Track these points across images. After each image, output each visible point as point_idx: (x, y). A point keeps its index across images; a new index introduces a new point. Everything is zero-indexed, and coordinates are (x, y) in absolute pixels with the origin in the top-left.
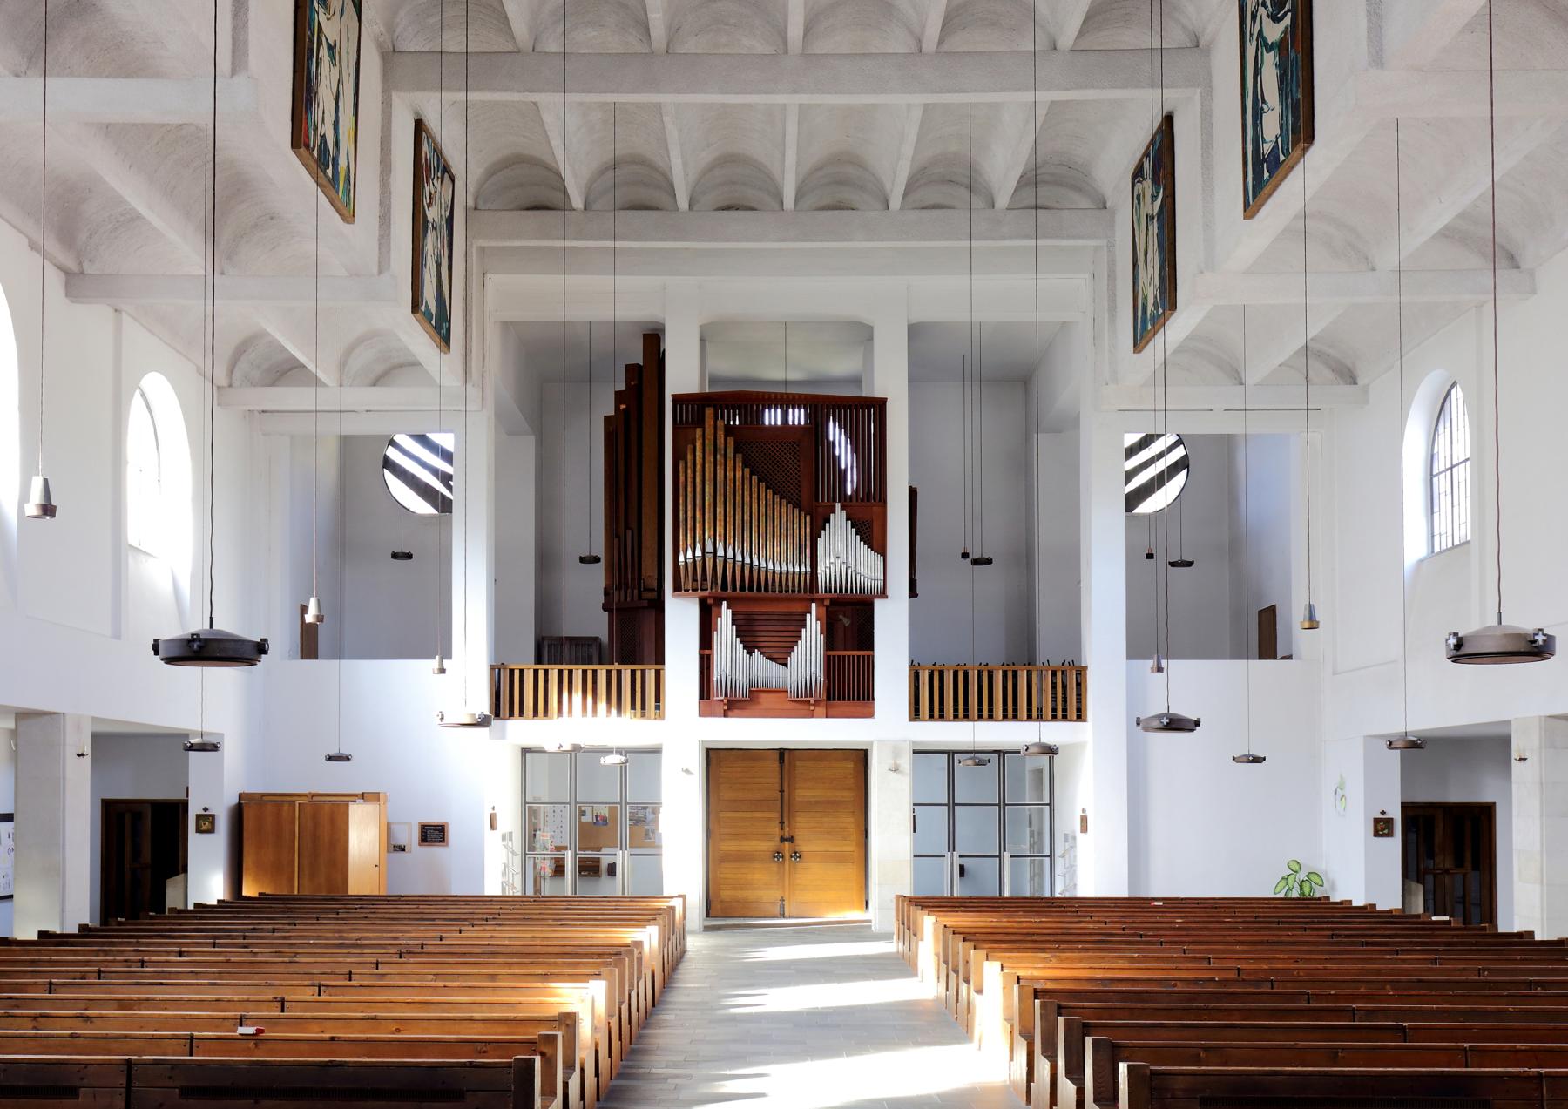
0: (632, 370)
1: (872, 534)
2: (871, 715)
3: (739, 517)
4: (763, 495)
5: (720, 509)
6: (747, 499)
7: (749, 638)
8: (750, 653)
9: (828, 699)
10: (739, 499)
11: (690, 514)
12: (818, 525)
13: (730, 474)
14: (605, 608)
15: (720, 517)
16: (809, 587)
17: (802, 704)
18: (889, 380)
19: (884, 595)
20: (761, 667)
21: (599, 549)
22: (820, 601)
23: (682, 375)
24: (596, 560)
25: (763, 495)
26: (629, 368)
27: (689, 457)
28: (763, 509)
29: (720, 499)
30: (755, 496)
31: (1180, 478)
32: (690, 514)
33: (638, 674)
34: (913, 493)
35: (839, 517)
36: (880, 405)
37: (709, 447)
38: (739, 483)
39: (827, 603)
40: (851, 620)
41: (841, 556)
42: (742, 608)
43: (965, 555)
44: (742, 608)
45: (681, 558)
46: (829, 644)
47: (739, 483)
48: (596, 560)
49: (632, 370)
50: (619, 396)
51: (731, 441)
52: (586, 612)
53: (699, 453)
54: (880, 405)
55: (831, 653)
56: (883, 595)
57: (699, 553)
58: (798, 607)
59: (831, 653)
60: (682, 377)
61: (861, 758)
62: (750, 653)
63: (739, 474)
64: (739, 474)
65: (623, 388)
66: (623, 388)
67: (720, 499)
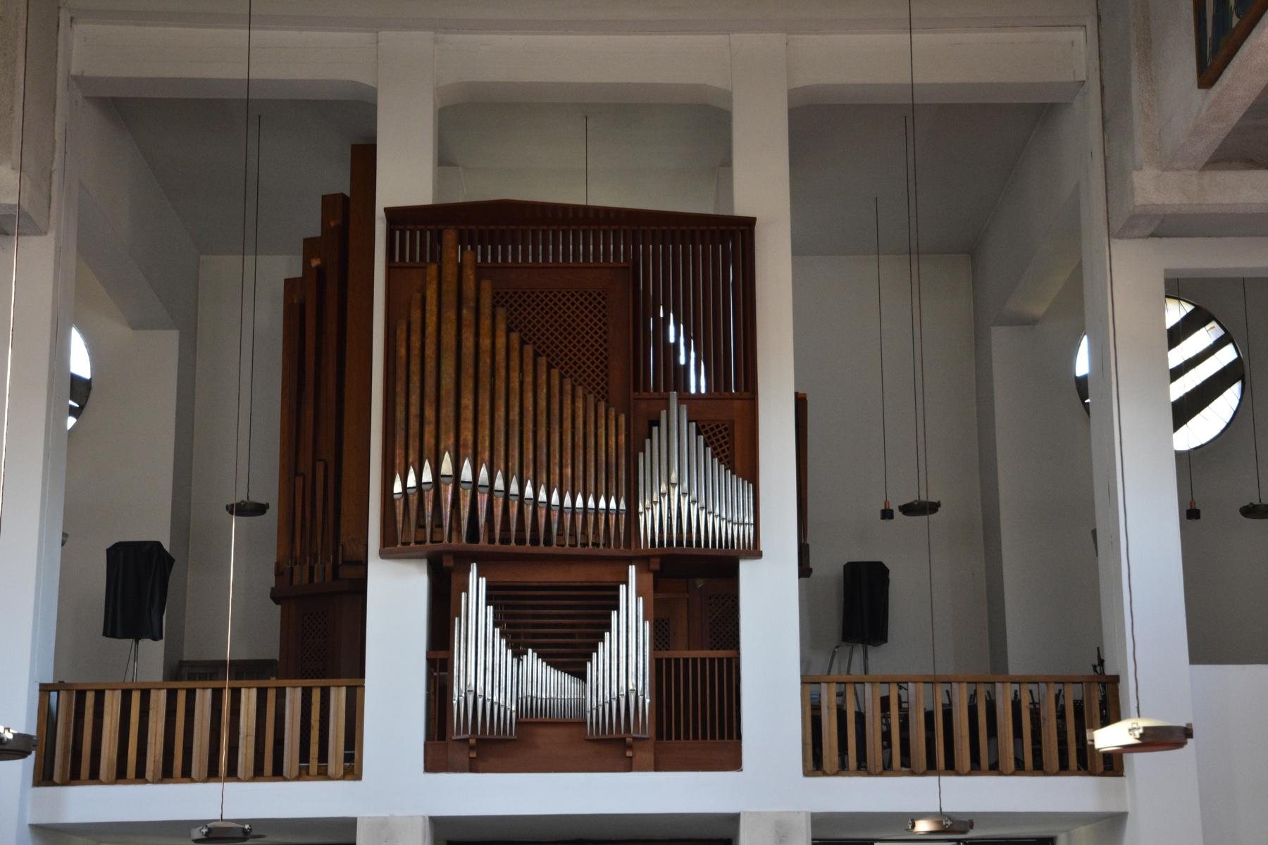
0: (331, 203)
1: (734, 449)
2: (735, 763)
3: (501, 413)
4: (543, 378)
5: (467, 401)
6: (515, 384)
7: (519, 631)
8: (518, 655)
9: (659, 735)
10: (501, 385)
11: (414, 410)
12: (642, 428)
13: (486, 342)
14: (276, 596)
15: (468, 414)
16: (621, 546)
17: (607, 746)
18: (760, 186)
19: (755, 552)
20: (543, 680)
21: (268, 490)
22: (642, 561)
23: (405, 180)
24: (260, 509)
25: (543, 378)
26: (328, 201)
27: (416, 315)
28: (543, 404)
29: (468, 384)
30: (529, 379)
31: (1229, 400)
32: (414, 410)
33: (316, 696)
34: (801, 404)
35: (677, 417)
36: (746, 226)
37: (450, 298)
38: (501, 356)
39: (655, 564)
40: (699, 588)
41: (681, 502)
42: (509, 575)
43: (887, 514)
44: (509, 575)
45: (398, 488)
46: (660, 638)
47: (501, 356)
48: (260, 509)
49: (331, 203)
50: (310, 247)
51: (486, 285)
52: (232, 598)
53: (432, 307)
54: (746, 226)
55: (664, 654)
56: (755, 552)
57: (427, 476)
58: (601, 574)
59: (664, 654)
60: (405, 180)
61: (815, 764)
62: (518, 655)
63: (501, 342)
64: (501, 342)
65: (317, 232)
66: (317, 232)
67: (468, 384)
